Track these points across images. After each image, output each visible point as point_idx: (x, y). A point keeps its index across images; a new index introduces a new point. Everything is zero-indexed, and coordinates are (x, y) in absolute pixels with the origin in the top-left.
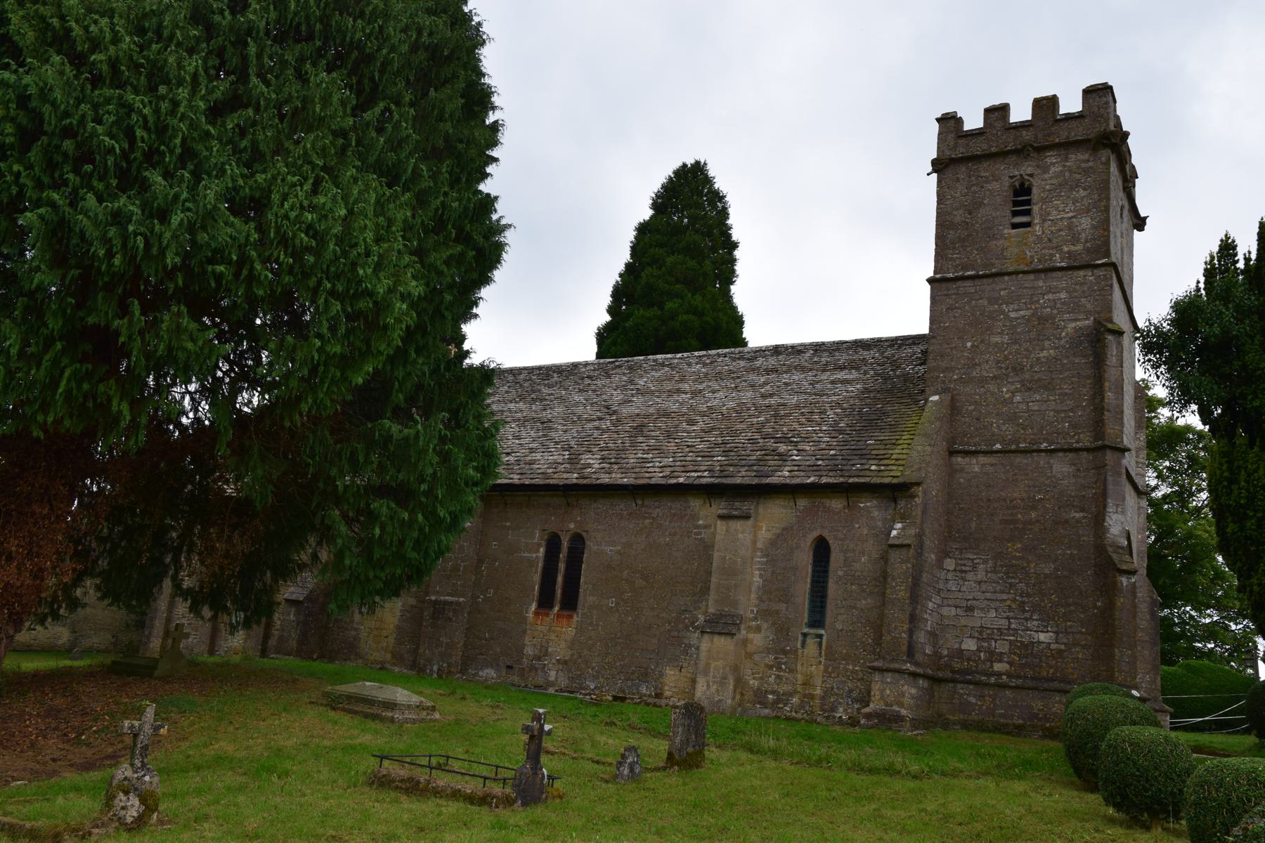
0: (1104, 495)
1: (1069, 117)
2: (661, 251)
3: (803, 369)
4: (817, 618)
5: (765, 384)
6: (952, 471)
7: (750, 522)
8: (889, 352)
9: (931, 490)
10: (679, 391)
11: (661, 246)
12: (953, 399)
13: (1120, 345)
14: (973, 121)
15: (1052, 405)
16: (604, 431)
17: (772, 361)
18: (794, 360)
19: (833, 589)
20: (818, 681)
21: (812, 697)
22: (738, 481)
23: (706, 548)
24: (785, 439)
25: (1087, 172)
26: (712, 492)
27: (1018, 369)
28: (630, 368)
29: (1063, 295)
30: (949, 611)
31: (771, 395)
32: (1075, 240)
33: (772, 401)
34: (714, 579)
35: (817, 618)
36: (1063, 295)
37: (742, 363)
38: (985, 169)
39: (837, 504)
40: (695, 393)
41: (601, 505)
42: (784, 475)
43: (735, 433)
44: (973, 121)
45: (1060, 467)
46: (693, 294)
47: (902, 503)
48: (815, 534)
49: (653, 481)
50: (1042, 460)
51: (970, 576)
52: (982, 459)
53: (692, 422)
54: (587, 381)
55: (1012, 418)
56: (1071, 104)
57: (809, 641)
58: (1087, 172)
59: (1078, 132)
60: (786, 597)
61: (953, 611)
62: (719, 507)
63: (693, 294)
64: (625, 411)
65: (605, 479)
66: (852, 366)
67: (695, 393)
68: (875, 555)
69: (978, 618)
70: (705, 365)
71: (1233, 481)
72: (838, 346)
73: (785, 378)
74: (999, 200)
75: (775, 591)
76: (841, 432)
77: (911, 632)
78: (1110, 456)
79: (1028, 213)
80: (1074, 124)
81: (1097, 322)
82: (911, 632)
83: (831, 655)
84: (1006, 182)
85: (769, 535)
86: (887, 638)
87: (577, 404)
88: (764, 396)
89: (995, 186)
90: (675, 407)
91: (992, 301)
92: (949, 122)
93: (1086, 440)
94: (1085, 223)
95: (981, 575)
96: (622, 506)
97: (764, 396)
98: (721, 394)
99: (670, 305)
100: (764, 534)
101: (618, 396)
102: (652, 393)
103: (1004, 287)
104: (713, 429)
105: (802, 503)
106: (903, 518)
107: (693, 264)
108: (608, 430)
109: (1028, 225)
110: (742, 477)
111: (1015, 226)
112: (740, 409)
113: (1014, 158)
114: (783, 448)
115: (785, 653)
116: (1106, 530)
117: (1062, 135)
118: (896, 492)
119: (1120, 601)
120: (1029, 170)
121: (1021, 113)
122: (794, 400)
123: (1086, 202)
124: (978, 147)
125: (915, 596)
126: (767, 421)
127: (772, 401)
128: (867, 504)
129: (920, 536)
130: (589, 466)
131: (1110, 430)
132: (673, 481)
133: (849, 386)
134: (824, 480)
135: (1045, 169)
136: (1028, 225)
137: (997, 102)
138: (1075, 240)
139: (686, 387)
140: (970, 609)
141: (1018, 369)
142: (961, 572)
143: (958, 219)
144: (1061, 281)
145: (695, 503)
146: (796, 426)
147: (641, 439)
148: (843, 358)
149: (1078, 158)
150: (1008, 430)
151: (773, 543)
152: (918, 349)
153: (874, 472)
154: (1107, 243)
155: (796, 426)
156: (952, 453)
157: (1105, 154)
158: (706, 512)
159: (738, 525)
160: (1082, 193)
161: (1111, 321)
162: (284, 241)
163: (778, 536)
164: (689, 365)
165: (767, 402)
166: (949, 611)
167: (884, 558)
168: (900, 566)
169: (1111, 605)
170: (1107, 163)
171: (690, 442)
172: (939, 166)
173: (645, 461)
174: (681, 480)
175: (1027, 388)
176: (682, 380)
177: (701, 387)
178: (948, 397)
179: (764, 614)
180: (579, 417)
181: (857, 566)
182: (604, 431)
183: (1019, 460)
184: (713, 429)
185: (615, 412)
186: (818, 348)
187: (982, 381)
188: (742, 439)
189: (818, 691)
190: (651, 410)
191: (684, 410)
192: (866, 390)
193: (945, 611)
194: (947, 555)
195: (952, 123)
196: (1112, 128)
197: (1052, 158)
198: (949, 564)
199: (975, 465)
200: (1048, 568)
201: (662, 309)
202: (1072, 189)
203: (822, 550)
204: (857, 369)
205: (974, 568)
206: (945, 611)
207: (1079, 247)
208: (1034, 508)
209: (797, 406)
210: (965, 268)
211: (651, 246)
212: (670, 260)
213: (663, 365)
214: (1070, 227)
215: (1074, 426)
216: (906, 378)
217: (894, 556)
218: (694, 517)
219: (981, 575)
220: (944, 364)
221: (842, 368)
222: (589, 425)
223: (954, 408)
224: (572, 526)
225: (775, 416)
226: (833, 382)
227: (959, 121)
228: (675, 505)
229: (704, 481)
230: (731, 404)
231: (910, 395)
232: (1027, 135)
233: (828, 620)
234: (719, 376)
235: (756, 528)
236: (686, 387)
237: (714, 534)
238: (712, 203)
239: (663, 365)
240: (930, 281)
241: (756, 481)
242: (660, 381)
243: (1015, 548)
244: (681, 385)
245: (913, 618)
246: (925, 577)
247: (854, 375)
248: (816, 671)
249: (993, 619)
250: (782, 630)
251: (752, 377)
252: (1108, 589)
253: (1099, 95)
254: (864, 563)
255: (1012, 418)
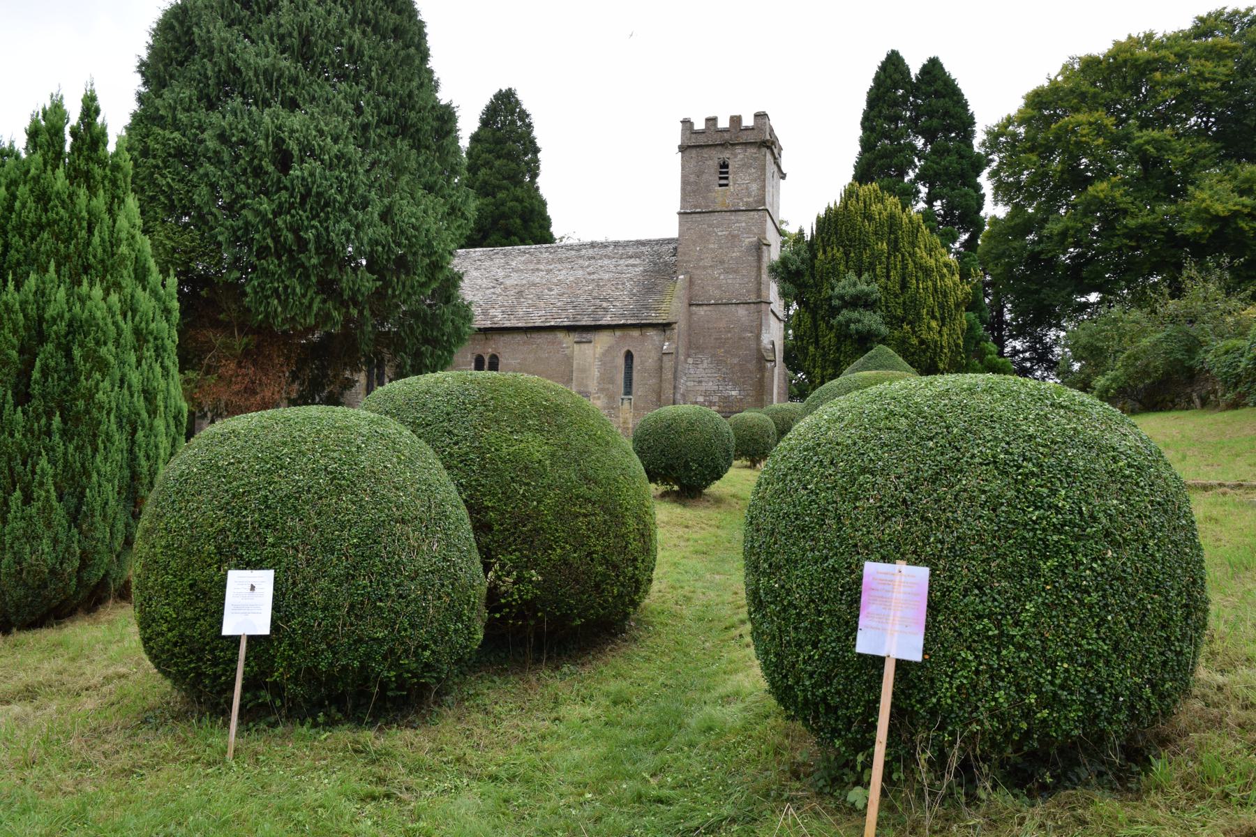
0: (761, 325)
1: (747, 129)
2: (491, 156)
3: (609, 257)
4: (628, 389)
5: (589, 266)
6: (691, 314)
7: (592, 345)
8: (656, 248)
9: (681, 327)
10: (538, 270)
11: (490, 152)
12: (691, 278)
13: (769, 251)
14: (699, 125)
15: (738, 281)
16: (499, 295)
17: (591, 252)
18: (603, 252)
19: (635, 376)
20: (630, 421)
21: (628, 429)
22: (584, 323)
23: (569, 359)
24: (605, 300)
25: (755, 159)
26: (570, 329)
27: (722, 262)
28: (504, 254)
29: (743, 224)
30: (690, 384)
31: (593, 273)
32: (749, 195)
33: (595, 277)
34: (574, 374)
35: (628, 389)
36: (743, 224)
37: (573, 253)
38: (706, 153)
39: (636, 333)
40: (549, 271)
41: (507, 338)
42: (607, 320)
43: (577, 296)
44: (699, 125)
45: (742, 311)
46: (515, 187)
47: (668, 332)
48: (626, 349)
49: (536, 325)
50: (733, 308)
51: (700, 366)
52: (705, 308)
53: (550, 290)
54: (479, 263)
55: (719, 287)
56: (748, 121)
57: (625, 401)
58: (755, 159)
59: (751, 137)
60: (612, 381)
61: (692, 383)
62: (575, 337)
63: (515, 187)
64: (508, 282)
65: (508, 324)
66: (636, 256)
67: (549, 271)
68: (656, 358)
69: (703, 387)
70: (551, 253)
71: (800, 325)
72: (627, 244)
73: (600, 262)
74: (713, 170)
75: (606, 378)
76: (634, 295)
77: (674, 394)
78: (763, 306)
79: (726, 178)
80: (749, 132)
81: (759, 239)
82: (674, 394)
83: (636, 408)
84: (716, 161)
85: (602, 351)
86: (663, 397)
87: (476, 278)
88: (589, 274)
89: (711, 162)
90: (538, 280)
91: (710, 226)
92: (687, 123)
93: (753, 298)
94: (754, 187)
95: (705, 365)
96: (519, 338)
97: (589, 274)
98: (564, 272)
99: (500, 195)
100: (599, 350)
101: (501, 274)
102: (522, 271)
103: (715, 218)
104: (564, 293)
105: (618, 333)
106: (669, 340)
107: (513, 165)
108: (500, 295)
109: (727, 185)
110: (586, 321)
111: (721, 185)
112: (577, 281)
113: (720, 148)
114: (605, 304)
115: (613, 408)
116: (761, 342)
117: (744, 137)
118: (665, 327)
119: (767, 374)
120: (728, 156)
121: (723, 123)
122: (607, 276)
123: (755, 175)
124: (702, 140)
125: (675, 378)
126: (594, 289)
127: (595, 277)
128: (651, 333)
129: (677, 348)
130: (496, 316)
131: (764, 293)
132: (548, 324)
133: (635, 269)
134: (629, 322)
135: (735, 156)
136: (727, 185)
137: (711, 115)
138: (749, 195)
139: (542, 267)
140: (700, 382)
141: (722, 262)
142: (695, 364)
143: (692, 180)
144: (743, 217)
145: (561, 335)
146: (610, 291)
147: (522, 300)
148: (631, 251)
149: (752, 151)
150: (717, 293)
151: (604, 354)
152: (671, 246)
153: (654, 318)
154: (764, 198)
155: (610, 291)
156: (691, 305)
157: (764, 150)
158: (567, 340)
159: (586, 346)
160: (753, 171)
161: (765, 239)
162: (402, 232)
163: (607, 351)
164: (541, 253)
165: (592, 277)
166: (690, 384)
167: (661, 360)
168: (668, 363)
169: (763, 376)
170: (765, 155)
171: (553, 301)
172: (683, 149)
173: (528, 313)
174: (552, 324)
175: (726, 271)
176: (539, 262)
177: (551, 267)
178: (688, 277)
179: (601, 390)
180: (480, 286)
181: (647, 364)
182: (499, 295)
183: (722, 308)
184: (564, 293)
185: (502, 283)
186: (616, 244)
187: (705, 268)
188: (581, 299)
189: (631, 426)
190: (524, 282)
191: (544, 282)
192: (645, 271)
193: (688, 384)
194: (689, 356)
195: (688, 124)
196: (768, 137)
197: (739, 150)
198: (690, 360)
199: (701, 311)
200: (736, 361)
201: (495, 197)
202: (748, 168)
203: (629, 356)
204: (639, 258)
205: (702, 362)
206: (688, 384)
207: (751, 199)
208: (729, 332)
209: (609, 280)
210: (696, 207)
211: (483, 152)
212: (497, 163)
213: (524, 252)
214: (747, 189)
215: (748, 291)
216: (666, 264)
217: (665, 358)
218: (560, 343)
219: (705, 365)
220: (686, 259)
221: (631, 257)
222: (488, 292)
223: (691, 282)
224: (490, 350)
225: (598, 286)
226: (627, 266)
227: (692, 124)
228: (549, 337)
229: (565, 324)
230: (572, 279)
231: (668, 274)
232: (727, 136)
233: (634, 391)
234: (560, 261)
235: (595, 347)
236: (542, 267)
237: (573, 352)
238: (522, 119)
239: (524, 252)
240: (679, 213)
241: (593, 323)
242: (525, 263)
243: (721, 352)
244: (538, 266)
245: (675, 388)
246: (680, 367)
247: (637, 261)
248: (630, 416)
249: (711, 386)
250: (611, 398)
251: (581, 261)
252: (762, 369)
253: (761, 116)
254: (651, 362)
255: (719, 287)
